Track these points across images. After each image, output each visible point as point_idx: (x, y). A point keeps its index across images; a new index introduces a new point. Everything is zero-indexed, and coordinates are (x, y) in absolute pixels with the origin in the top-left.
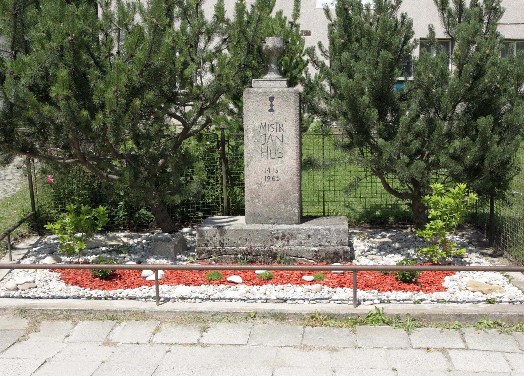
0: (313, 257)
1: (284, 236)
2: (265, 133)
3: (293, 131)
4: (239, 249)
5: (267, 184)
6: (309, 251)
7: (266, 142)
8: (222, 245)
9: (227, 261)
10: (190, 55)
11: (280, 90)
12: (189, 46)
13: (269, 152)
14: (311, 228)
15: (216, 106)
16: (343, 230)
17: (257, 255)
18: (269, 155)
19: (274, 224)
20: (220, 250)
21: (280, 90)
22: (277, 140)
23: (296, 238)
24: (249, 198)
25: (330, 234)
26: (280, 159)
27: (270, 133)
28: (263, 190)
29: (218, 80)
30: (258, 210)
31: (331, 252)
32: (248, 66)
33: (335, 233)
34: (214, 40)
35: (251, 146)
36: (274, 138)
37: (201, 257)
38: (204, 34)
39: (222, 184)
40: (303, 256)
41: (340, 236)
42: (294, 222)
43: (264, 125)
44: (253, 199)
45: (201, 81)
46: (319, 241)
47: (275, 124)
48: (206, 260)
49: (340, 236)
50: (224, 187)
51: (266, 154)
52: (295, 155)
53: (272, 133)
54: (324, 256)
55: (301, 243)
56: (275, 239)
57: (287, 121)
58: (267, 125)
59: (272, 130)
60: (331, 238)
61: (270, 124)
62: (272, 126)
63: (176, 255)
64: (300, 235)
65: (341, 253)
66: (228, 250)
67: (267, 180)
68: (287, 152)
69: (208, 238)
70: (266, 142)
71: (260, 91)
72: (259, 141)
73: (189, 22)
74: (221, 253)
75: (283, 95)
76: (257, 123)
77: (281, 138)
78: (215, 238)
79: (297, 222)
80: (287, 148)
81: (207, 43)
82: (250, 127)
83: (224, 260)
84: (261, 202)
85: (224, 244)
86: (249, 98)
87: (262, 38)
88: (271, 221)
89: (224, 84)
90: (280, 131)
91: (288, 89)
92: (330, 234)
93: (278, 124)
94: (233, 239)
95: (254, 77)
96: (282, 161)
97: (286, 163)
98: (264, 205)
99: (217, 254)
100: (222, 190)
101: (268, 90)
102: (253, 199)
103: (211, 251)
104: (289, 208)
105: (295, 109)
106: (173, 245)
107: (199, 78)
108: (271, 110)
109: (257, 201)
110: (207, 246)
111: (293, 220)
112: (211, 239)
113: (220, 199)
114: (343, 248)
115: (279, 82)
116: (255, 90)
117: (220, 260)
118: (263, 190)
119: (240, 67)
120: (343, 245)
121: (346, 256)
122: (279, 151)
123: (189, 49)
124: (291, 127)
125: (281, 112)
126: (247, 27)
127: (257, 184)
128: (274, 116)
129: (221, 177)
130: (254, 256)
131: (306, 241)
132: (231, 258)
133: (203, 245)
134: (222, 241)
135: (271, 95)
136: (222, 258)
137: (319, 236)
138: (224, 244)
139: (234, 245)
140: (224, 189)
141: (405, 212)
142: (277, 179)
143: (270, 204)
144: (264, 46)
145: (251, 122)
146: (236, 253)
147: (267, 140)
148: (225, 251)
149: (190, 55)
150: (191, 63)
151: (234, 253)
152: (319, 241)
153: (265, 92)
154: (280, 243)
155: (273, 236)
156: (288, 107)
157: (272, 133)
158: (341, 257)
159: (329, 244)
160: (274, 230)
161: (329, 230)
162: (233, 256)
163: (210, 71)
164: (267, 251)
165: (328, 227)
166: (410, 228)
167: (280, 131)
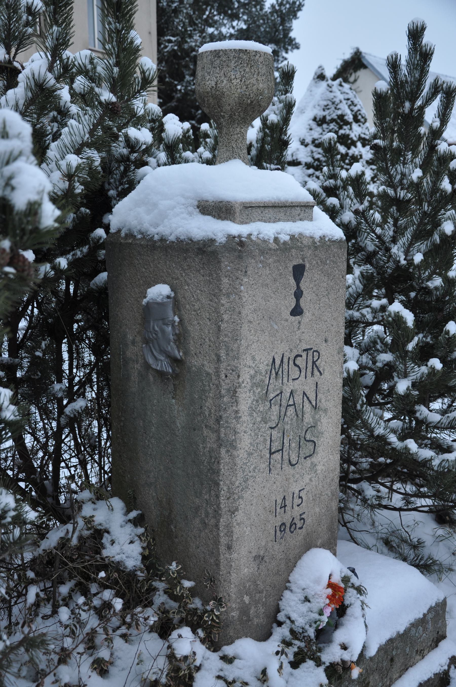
18: (286, 457)
43: (278, 362)
58: (285, 360)
167: (312, 374)
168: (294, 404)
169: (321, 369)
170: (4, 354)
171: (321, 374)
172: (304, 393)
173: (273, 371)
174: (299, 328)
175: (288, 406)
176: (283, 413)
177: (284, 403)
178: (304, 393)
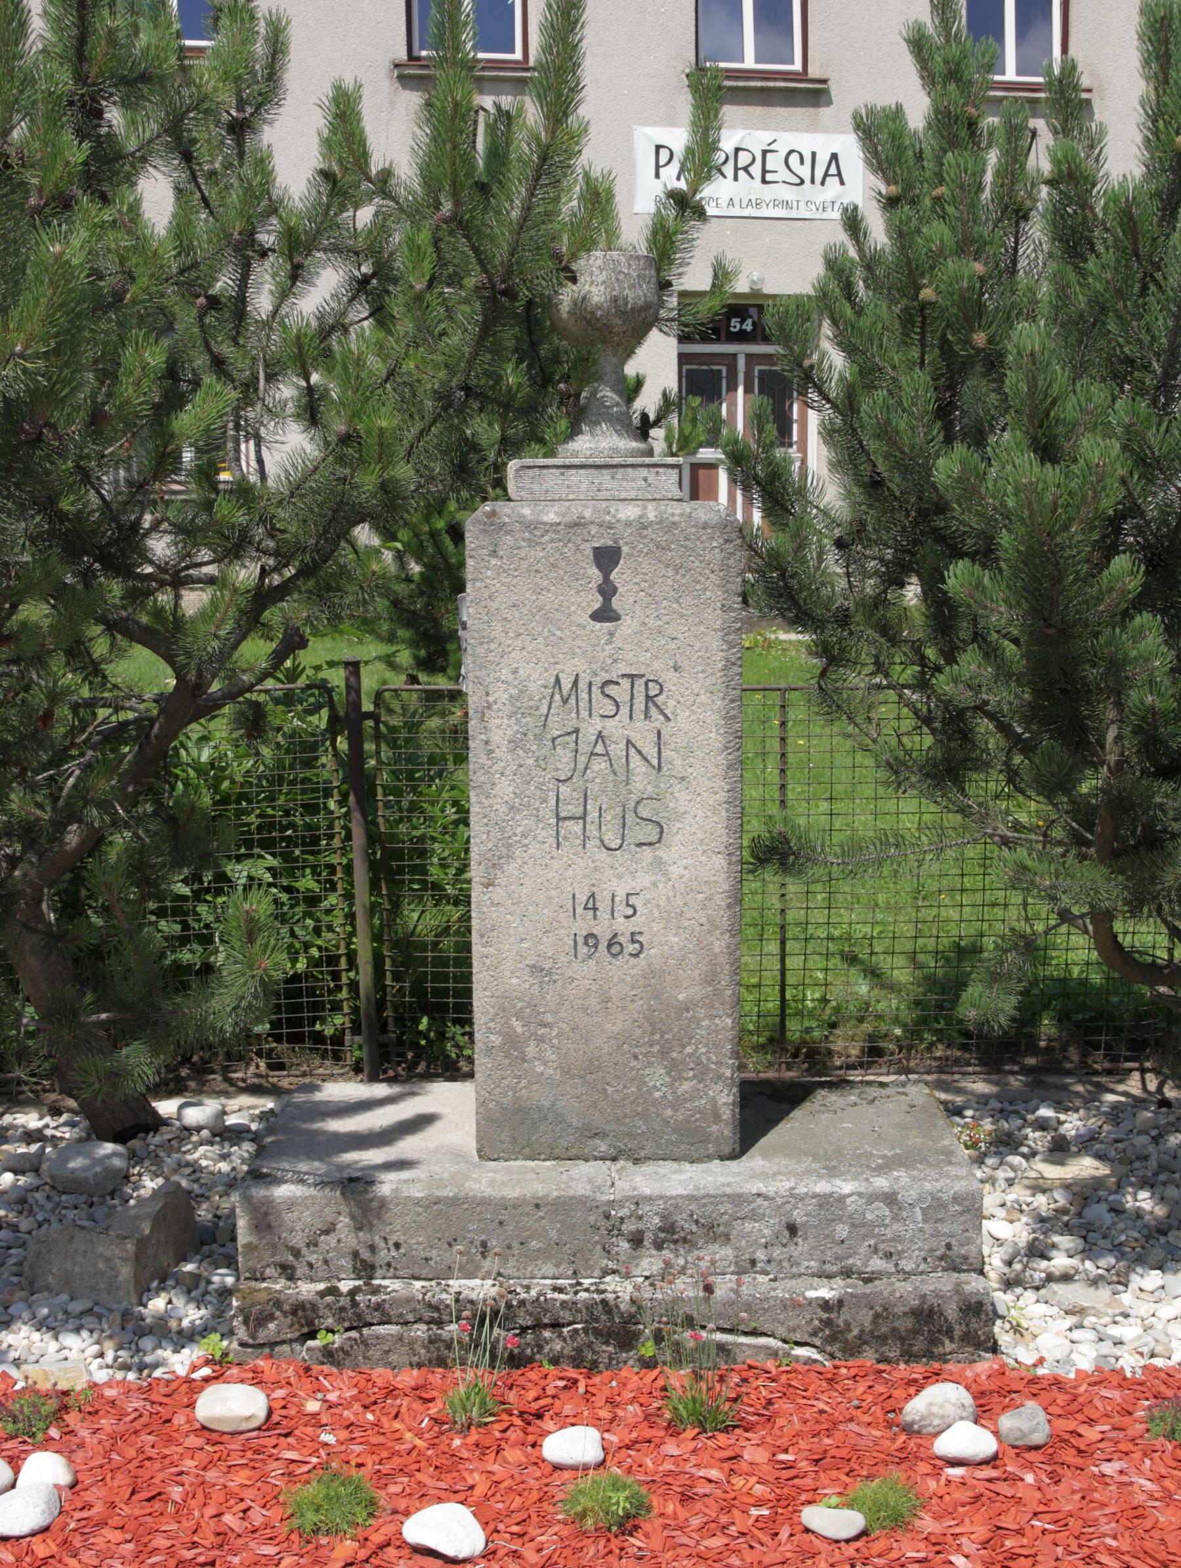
0: (814, 1334)
1: (669, 1228)
2: (571, 724)
3: (713, 718)
4: (448, 1298)
5: (584, 970)
6: (795, 1305)
7: (579, 771)
8: (365, 1269)
9: (393, 1357)
10: (207, 345)
11: (651, 516)
12: (202, 300)
13: (593, 815)
14: (801, 1190)
15: (329, 588)
16: (956, 1199)
17: (538, 1326)
18: (592, 829)
19: (614, 1159)
20: (355, 1304)
21: (651, 516)
22: (635, 759)
23: (727, 1238)
24: (496, 1040)
25: (896, 1218)
26: (647, 852)
27: (597, 724)
28: (562, 1000)
29: (341, 460)
30: (540, 1097)
31: (900, 1310)
32: (485, 399)
33: (919, 1215)
34: (318, 282)
35: (505, 789)
36: (618, 750)
37: (263, 1335)
38: (272, 257)
39: (349, 896)
40: (767, 1327)
41: (945, 1228)
42: (712, 1149)
43: (567, 684)
44: (513, 1042)
45: (260, 461)
46: (840, 1250)
47: (626, 684)
48: (285, 1348)
49: (945, 1228)
50: (358, 909)
51: (577, 827)
52: (721, 830)
53: (611, 727)
54: (868, 1326)
55: (753, 1262)
56: (626, 1245)
57: (685, 664)
58: (583, 685)
59: (610, 709)
60: (897, 1239)
61: (598, 681)
62: (611, 690)
63: (143, 1293)
64: (748, 1226)
65: (951, 1311)
66: (396, 1302)
67: (583, 950)
68: (680, 817)
69: (298, 1240)
70: (579, 771)
71: (551, 517)
72: (542, 763)
73: (204, 199)
74: (359, 1316)
75: (662, 538)
76: (537, 679)
77: (650, 751)
78: (331, 1240)
79: (727, 1150)
80: (681, 799)
81: (284, 294)
82: (500, 695)
83: (374, 1353)
84: (550, 1055)
85: (373, 1267)
86: (494, 553)
87: (558, 257)
88: (603, 1147)
89: (368, 481)
90: (647, 716)
91: (687, 507)
92: (896, 1218)
93: (640, 684)
94: (417, 1243)
95: (510, 446)
96: (658, 862)
97: (675, 871)
98: (566, 1071)
99: (341, 1320)
100: (351, 917)
101: (588, 513)
102: (513, 1042)
103: (314, 1307)
104: (686, 1086)
105: (725, 609)
106: (130, 1247)
107: (247, 449)
108: (605, 614)
109: (531, 1051)
110: (291, 1278)
111: (705, 1138)
112: (313, 1244)
113: (343, 960)
114: (958, 1289)
115: (644, 472)
116: (526, 511)
117: (358, 1351)
118: (562, 1000)
119: (444, 399)
120: (956, 1269)
121: (974, 1325)
122: (644, 814)
123: (201, 318)
124: (704, 698)
125: (653, 623)
126: (485, 210)
127: (535, 969)
128: (618, 643)
129: (348, 869)
130: (524, 1330)
131: (777, 1252)
132: (412, 1343)
133: (269, 1272)
134: (365, 1254)
135: (605, 541)
136: (365, 1342)
137: (842, 1231)
138: (373, 1267)
139: (424, 1273)
140: (360, 922)
141: (1084, 982)
142: (631, 948)
143: (593, 1065)
144: (567, 296)
145: (505, 674)
146: (436, 1315)
147: (582, 759)
148: (379, 1307)
149: (207, 345)
150: (208, 379)
151: (427, 1315)
152: (840, 1250)
153: (577, 524)
154: (650, 1263)
155: (615, 1230)
156: (687, 600)
157: (611, 727)
158: (949, 1333)
159: (890, 1267)
160: (620, 1203)
161: (890, 1199)
162: (420, 1331)
163: (298, 417)
164: (590, 1307)
165: (881, 1183)
166: (1136, 1075)
167: (647, 716)
168: (607, 754)
169: (668, 712)
170: (153, 354)
171: (668, 719)
172: (629, 742)
173: (557, 697)
174: (609, 642)
175: (592, 754)
176: (581, 766)
177: (584, 748)
178: (629, 742)
